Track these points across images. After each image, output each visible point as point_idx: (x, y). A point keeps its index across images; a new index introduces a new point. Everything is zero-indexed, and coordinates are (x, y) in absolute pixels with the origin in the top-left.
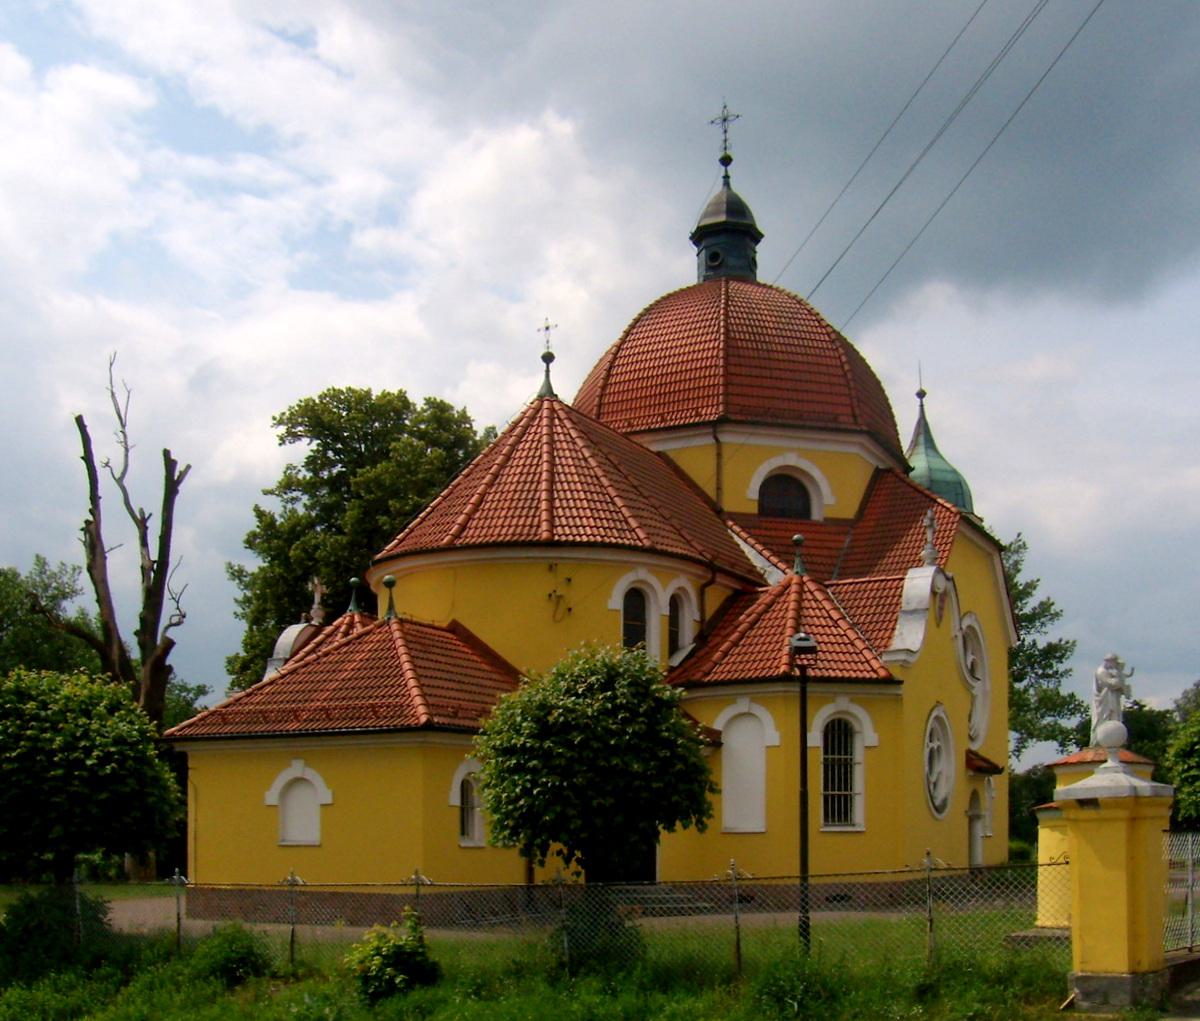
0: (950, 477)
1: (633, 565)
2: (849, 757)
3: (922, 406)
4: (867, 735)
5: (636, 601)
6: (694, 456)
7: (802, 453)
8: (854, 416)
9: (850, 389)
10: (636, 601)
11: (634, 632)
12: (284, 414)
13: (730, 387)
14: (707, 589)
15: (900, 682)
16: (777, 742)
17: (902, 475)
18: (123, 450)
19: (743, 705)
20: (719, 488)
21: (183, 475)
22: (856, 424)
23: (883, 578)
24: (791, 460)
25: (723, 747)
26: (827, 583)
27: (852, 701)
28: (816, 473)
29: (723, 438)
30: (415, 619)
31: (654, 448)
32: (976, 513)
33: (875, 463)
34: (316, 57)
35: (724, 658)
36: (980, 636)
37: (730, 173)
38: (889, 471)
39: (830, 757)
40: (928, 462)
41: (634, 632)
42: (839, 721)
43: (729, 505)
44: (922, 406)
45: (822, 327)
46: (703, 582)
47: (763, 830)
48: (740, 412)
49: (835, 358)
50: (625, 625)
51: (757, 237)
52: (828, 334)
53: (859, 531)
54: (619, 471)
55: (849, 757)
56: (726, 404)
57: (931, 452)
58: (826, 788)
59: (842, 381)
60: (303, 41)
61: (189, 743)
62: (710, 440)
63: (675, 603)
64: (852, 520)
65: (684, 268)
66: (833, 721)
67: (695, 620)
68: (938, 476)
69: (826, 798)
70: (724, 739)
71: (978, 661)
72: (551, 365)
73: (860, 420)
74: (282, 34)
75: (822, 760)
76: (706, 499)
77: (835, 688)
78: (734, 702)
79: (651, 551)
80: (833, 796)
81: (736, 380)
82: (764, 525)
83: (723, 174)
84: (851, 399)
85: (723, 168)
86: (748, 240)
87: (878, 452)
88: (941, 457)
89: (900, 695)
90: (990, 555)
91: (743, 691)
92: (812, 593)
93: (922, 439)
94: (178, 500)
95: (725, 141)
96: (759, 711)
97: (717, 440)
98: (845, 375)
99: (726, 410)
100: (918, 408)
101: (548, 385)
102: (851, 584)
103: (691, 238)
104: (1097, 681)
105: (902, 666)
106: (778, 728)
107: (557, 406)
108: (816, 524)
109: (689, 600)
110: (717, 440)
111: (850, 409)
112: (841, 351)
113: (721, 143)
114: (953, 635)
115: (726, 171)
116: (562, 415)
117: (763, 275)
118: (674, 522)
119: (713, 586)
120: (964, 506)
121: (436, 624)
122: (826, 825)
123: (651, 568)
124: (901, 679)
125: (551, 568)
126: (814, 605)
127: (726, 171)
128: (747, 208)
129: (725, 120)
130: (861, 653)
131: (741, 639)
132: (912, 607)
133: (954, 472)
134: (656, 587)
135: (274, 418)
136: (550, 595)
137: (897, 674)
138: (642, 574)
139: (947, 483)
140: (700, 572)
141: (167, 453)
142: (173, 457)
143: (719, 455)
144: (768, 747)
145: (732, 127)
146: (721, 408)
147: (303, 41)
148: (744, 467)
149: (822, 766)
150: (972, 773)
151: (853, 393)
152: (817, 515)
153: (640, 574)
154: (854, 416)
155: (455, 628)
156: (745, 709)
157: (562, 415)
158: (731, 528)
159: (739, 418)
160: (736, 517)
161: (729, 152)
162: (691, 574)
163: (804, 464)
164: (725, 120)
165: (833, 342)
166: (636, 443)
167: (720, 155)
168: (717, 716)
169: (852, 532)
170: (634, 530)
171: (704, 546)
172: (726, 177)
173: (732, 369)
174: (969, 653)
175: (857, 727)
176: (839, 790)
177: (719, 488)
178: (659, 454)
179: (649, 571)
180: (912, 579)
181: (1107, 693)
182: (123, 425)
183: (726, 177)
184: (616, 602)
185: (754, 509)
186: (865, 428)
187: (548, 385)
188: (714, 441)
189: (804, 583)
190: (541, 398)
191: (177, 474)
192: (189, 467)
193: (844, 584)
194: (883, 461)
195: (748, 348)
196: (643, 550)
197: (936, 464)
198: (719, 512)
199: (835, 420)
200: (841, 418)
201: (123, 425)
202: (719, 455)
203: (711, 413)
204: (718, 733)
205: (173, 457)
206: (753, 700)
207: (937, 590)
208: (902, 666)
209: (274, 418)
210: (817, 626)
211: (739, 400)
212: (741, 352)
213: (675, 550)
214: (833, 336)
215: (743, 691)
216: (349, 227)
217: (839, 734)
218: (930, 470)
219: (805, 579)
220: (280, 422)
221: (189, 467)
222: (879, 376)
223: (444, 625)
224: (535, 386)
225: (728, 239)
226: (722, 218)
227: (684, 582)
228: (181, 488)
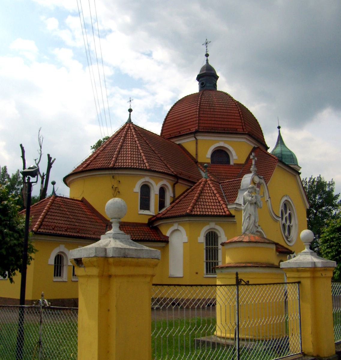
0: (289, 153)
1: (144, 176)
2: (216, 246)
3: (279, 131)
4: (223, 238)
5: (145, 189)
6: (188, 144)
7: (225, 142)
8: (243, 129)
9: (242, 120)
10: (145, 189)
11: (145, 205)
12: (94, 145)
13: (200, 121)
14: (176, 185)
15: (234, 216)
16: (187, 241)
17: (265, 151)
18: (40, 156)
19: (175, 227)
20: (197, 154)
21: (53, 161)
22: (244, 131)
23: (238, 179)
24: (221, 144)
25: (169, 242)
26: (220, 182)
27: (216, 224)
28: (230, 148)
29: (198, 138)
30: (65, 196)
31: (178, 143)
32: (299, 165)
33: (253, 146)
34: (153, 59)
35: (171, 209)
36: (292, 204)
37: (208, 59)
38: (258, 148)
39: (213, 247)
40: (281, 149)
41: (145, 205)
42: (212, 232)
43: (200, 160)
44: (279, 131)
45: (233, 101)
46: (175, 182)
47: (182, 276)
48: (203, 129)
49: (237, 111)
50: (141, 198)
51: (199, 78)
52: (235, 103)
53: (245, 167)
54: (148, 145)
55: (216, 246)
56: (199, 126)
57: (282, 145)
58: (207, 259)
59: (239, 118)
60: (150, 55)
61: (235, 266)
62: (194, 139)
63: (162, 191)
64: (243, 164)
65: (194, 88)
66: (209, 232)
67: (171, 197)
68: (283, 153)
69: (207, 263)
70: (170, 240)
71: (292, 213)
72: (131, 113)
73: (245, 130)
74: (144, 54)
75: (205, 248)
76: (191, 156)
77: (209, 219)
78: (172, 225)
79: (150, 170)
80: (210, 262)
81: (202, 118)
82: (214, 166)
83: (206, 59)
84: (242, 123)
85: (206, 58)
86: (213, 78)
87: (254, 142)
88: (286, 147)
89: (235, 221)
90: (295, 176)
91: (175, 221)
92: (209, 185)
93: (279, 142)
94: (52, 170)
95: (207, 49)
96: (181, 228)
97: (196, 139)
98: (240, 116)
99: (199, 129)
100: (278, 132)
101: (130, 120)
102: (228, 182)
103: (197, 79)
104: (244, 198)
105: (235, 210)
106: (187, 235)
107: (131, 125)
108: (231, 166)
109: (169, 190)
110: (196, 139)
111: (241, 126)
112: (239, 108)
113: (206, 50)
114: (266, 200)
115: (207, 58)
116: (132, 128)
117: (219, 89)
118: (165, 162)
119: (178, 184)
120: (294, 163)
121: (75, 199)
122: (207, 274)
123: (151, 177)
124: (234, 215)
125: (113, 177)
126: (208, 189)
127: (207, 58)
128: (214, 69)
129: (206, 43)
130: (222, 205)
131: (180, 202)
132: (244, 187)
133: (290, 151)
134: (153, 184)
135: (91, 147)
136: (112, 187)
137: (233, 213)
138: (147, 179)
139: (288, 155)
140: (173, 179)
141: (49, 155)
142: (51, 156)
143: (197, 143)
144: (184, 243)
145: (208, 45)
146: (197, 128)
147: (150, 55)
148: (204, 148)
149: (205, 250)
150: (278, 254)
151: (243, 121)
152: (232, 163)
153: (147, 179)
154: (243, 129)
155: (83, 201)
156: (176, 228)
157: (132, 128)
158: (199, 167)
159: (203, 130)
160: (202, 164)
161: (208, 53)
162: (170, 180)
163: (226, 146)
164: (206, 43)
165: (236, 106)
166: (172, 142)
167: (205, 53)
168: (203, 228)
169: (243, 167)
170: (145, 164)
171: (174, 169)
172: (207, 60)
173: (201, 115)
174: (288, 210)
175: (219, 235)
176: (212, 260)
177: (197, 154)
178: (179, 145)
179: (150, 178)
180: (245, 178)
181: (248, 204)
182: (41, 148)
183: (207, 60)
184: (137, 189)
185: (209, 161)
186: (247, 133)
187: (130, 120)
188: (195, 139)
189: (207, 181)
190: (127, 123)
191: (51, 161)
192: (55, 159)
193: (226, 182)
194: (257, 145)
195: (207, 108)
196: (146, 170)
197: (284, 149)
198: (196, 162)
199: (237, 130)
200: (238, 130)
201: (41, 148)
202: (197, 143)
203: (193, 130)
204: (168, 237)
205: (51, 156)
206: (179, 224)
207: (255, 182)
208: (235, 210)
209: (91, 147)
210: (207, 196)
211: (203, 125)
212: (204, 110)
213: (159, 170)
214: (237, 104)
215: (175, 221)
216: (162, 106)
217: (212, 237)
218: (282, 151)
219: (208, 180)
220: (93, 148)
221: (55, 159)
222: (257, 118)
223: (80, 199)
224: (126, 120)
225: (208, 77)
226: (205, 72)
227: (166, 182)
228: (52, 165)
